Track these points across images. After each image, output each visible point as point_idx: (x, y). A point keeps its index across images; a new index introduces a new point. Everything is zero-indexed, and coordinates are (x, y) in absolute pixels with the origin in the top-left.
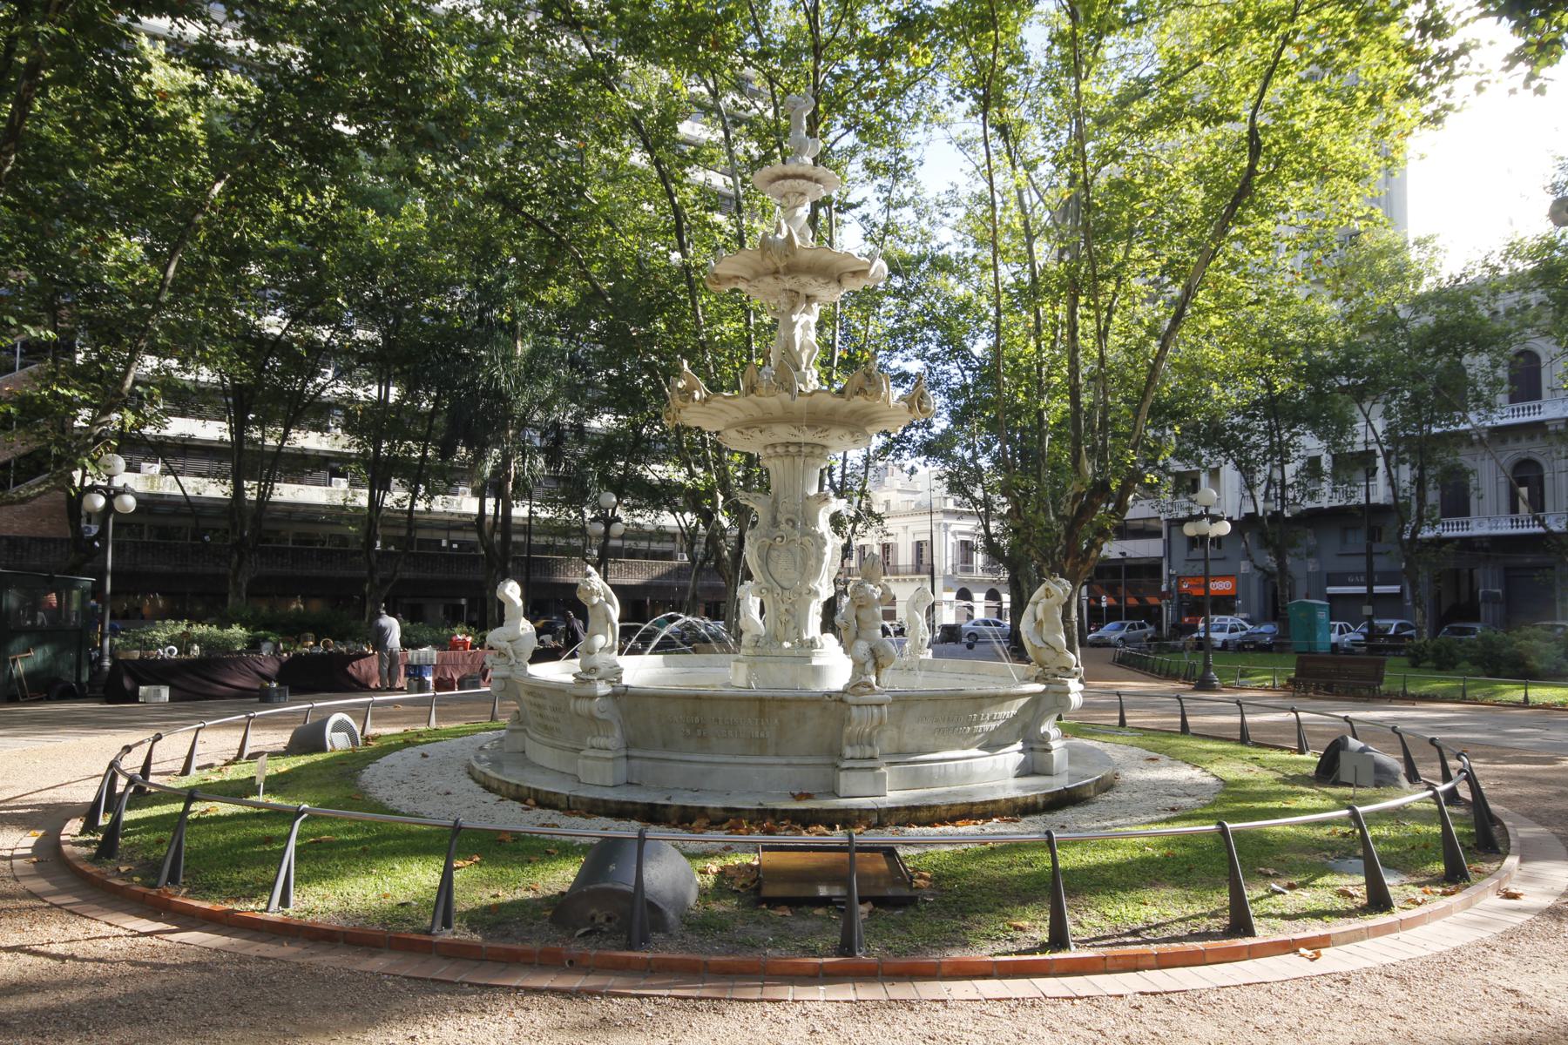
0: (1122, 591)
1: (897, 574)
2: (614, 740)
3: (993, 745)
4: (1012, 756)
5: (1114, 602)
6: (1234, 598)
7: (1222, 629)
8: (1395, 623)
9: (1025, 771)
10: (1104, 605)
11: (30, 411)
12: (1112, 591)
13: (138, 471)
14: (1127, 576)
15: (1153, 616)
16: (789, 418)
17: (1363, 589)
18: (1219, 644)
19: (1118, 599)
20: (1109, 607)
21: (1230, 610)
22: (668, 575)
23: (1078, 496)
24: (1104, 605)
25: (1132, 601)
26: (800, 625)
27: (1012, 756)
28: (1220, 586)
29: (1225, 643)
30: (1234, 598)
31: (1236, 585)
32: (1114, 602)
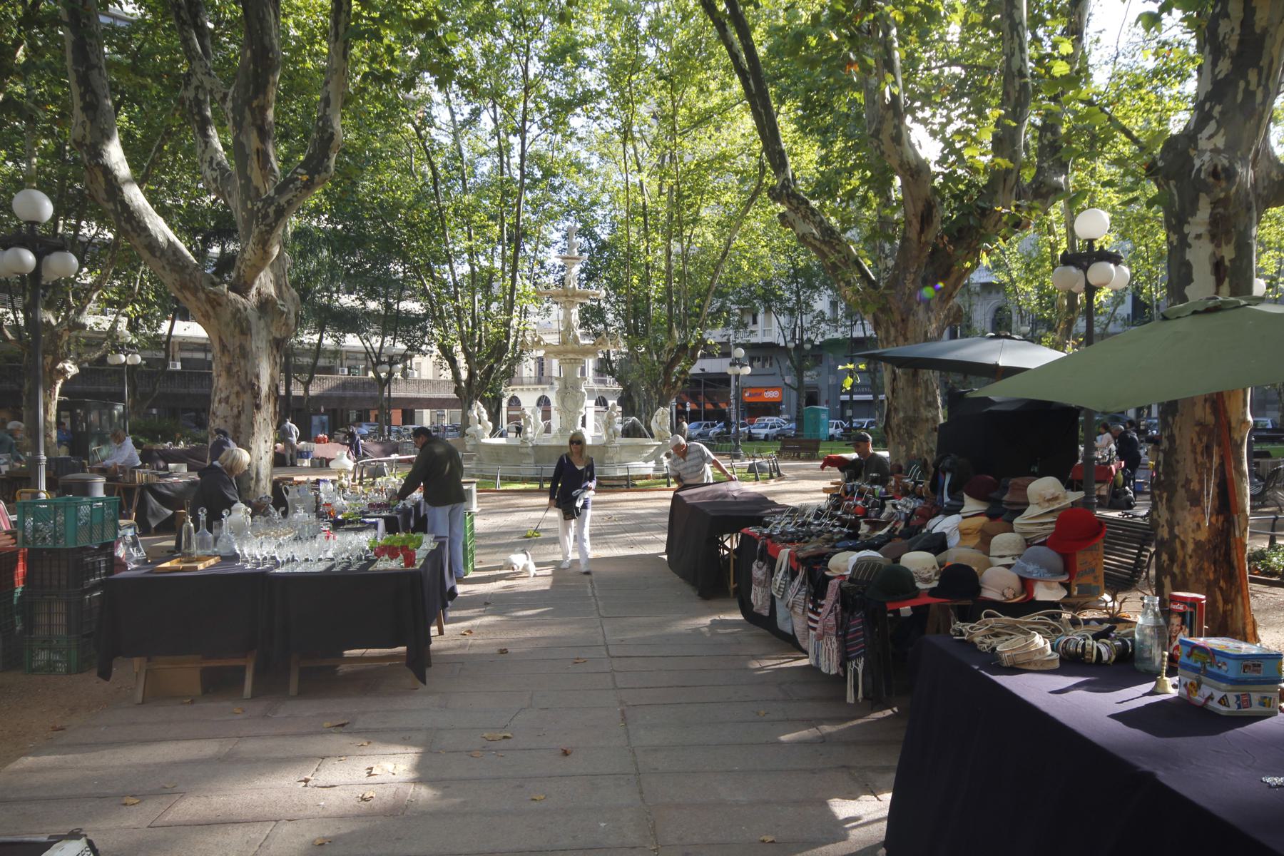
0: (702, 398)
1: (522, 384)
2: (532, 461)
3: (646, 461)
4: (652, 464)
5: (695, 407)
6: (780, 403)
7: (763, 427)
8: (867, 421)
9: (656, 469)
10: (688, 409)
11: (32, 289)
12: (694, 397)
13: (538, 405)
14: (706, 385)
15: (722, 416)
16: (573, 352)
17: (870, 397)
18: (762, 437)
19: (699, 405)
20: (692, 411)
21: (778, 413)
22: (337, 387)
23: (671, 350)
24: (688, 409)
25: (709, 406)
26: (575, 425)
27: (652, 464)
28: (772, 395)
29: (767, 436)
30: (780, 403)
31: (782, 394)
32: (695, 407)
